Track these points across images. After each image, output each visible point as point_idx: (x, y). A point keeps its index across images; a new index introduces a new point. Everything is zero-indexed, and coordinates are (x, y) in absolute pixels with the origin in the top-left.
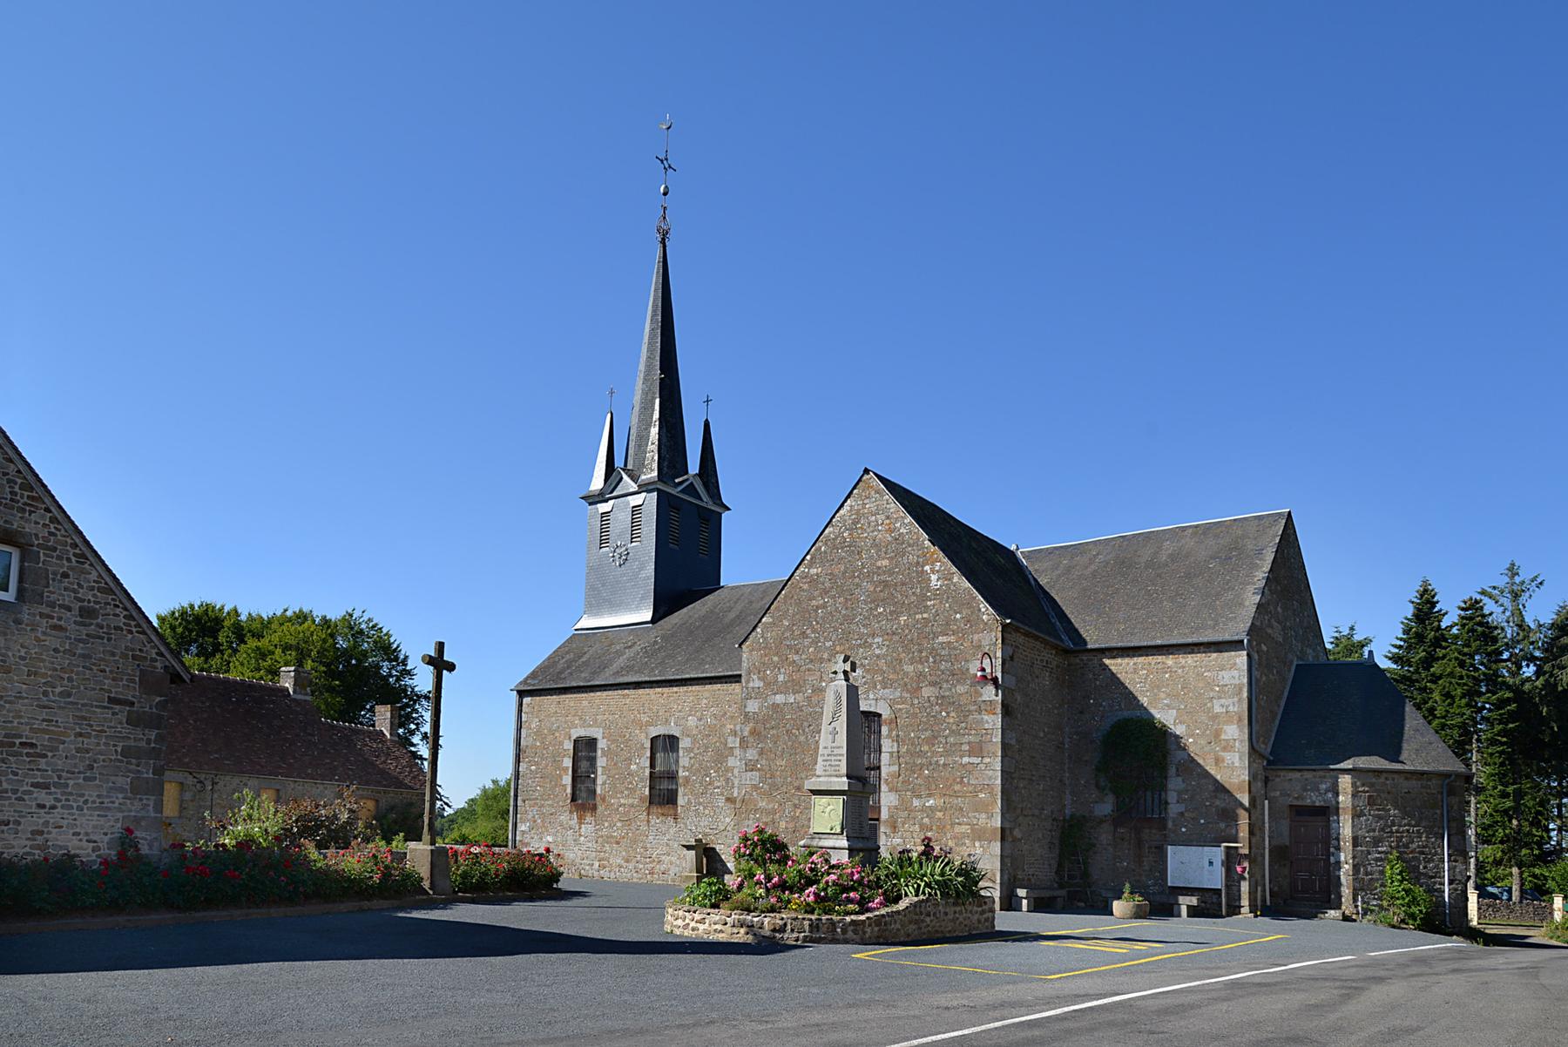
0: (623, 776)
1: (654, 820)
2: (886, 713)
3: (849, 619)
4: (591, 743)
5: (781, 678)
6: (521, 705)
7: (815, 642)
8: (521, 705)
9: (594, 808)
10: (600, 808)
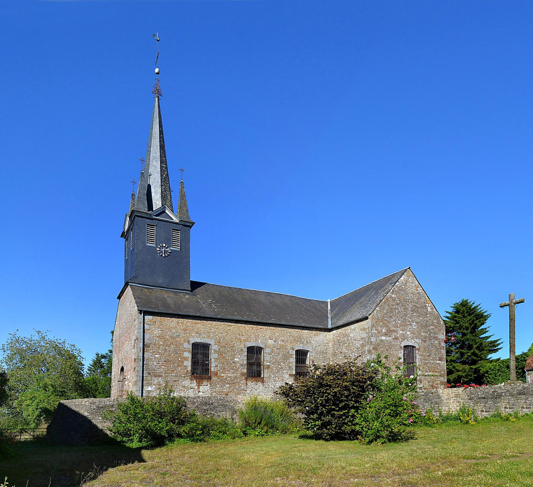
0: (228, 361)
1: (249, 383)
2: (417, 347)
3: (405, 315)
4: (206, 347)
5: (384, 331)
6: (144, 319)
7: (395, 320)
8: (144, 319)
9: (210, 378)
10: (214, 378)
